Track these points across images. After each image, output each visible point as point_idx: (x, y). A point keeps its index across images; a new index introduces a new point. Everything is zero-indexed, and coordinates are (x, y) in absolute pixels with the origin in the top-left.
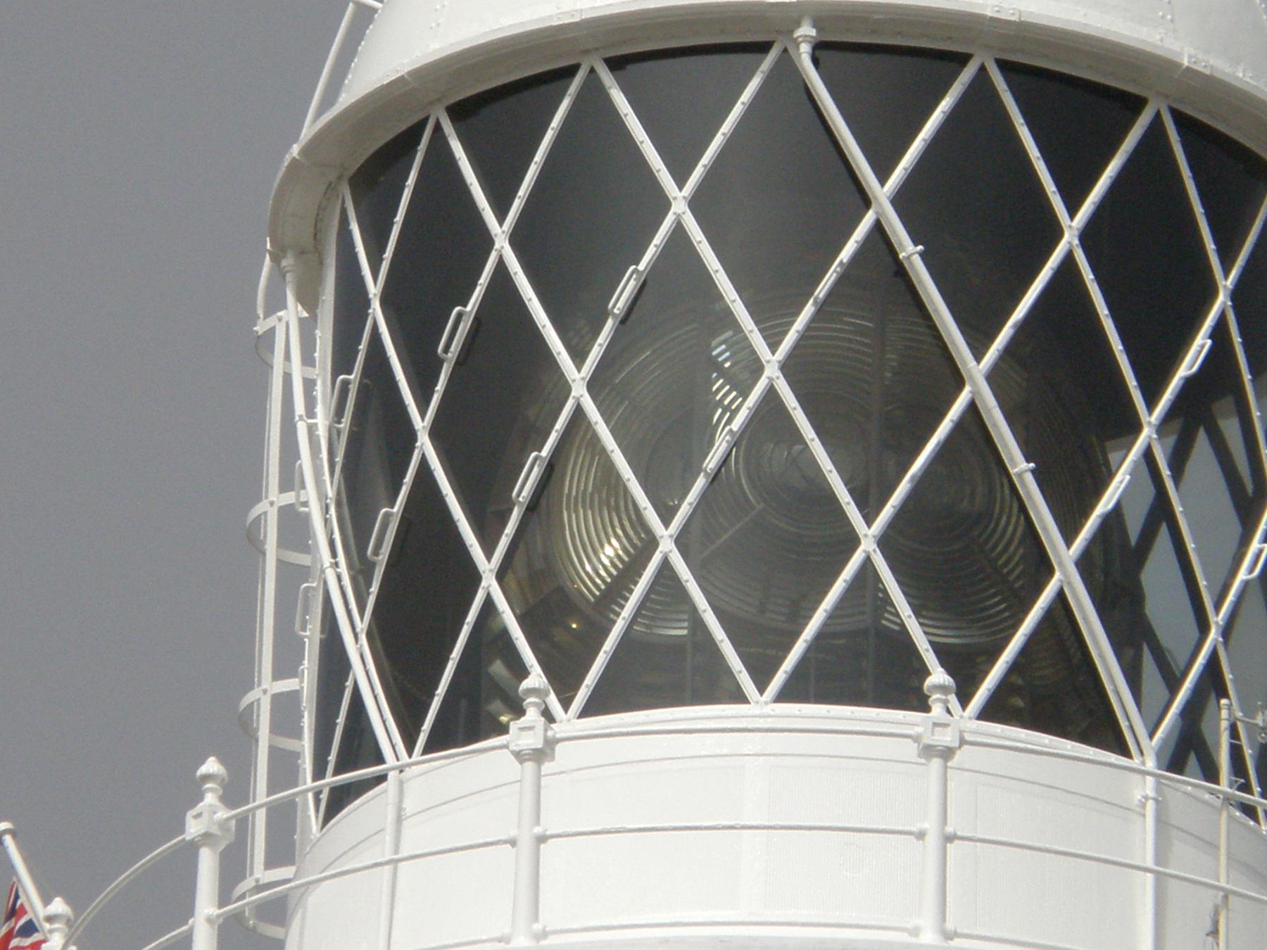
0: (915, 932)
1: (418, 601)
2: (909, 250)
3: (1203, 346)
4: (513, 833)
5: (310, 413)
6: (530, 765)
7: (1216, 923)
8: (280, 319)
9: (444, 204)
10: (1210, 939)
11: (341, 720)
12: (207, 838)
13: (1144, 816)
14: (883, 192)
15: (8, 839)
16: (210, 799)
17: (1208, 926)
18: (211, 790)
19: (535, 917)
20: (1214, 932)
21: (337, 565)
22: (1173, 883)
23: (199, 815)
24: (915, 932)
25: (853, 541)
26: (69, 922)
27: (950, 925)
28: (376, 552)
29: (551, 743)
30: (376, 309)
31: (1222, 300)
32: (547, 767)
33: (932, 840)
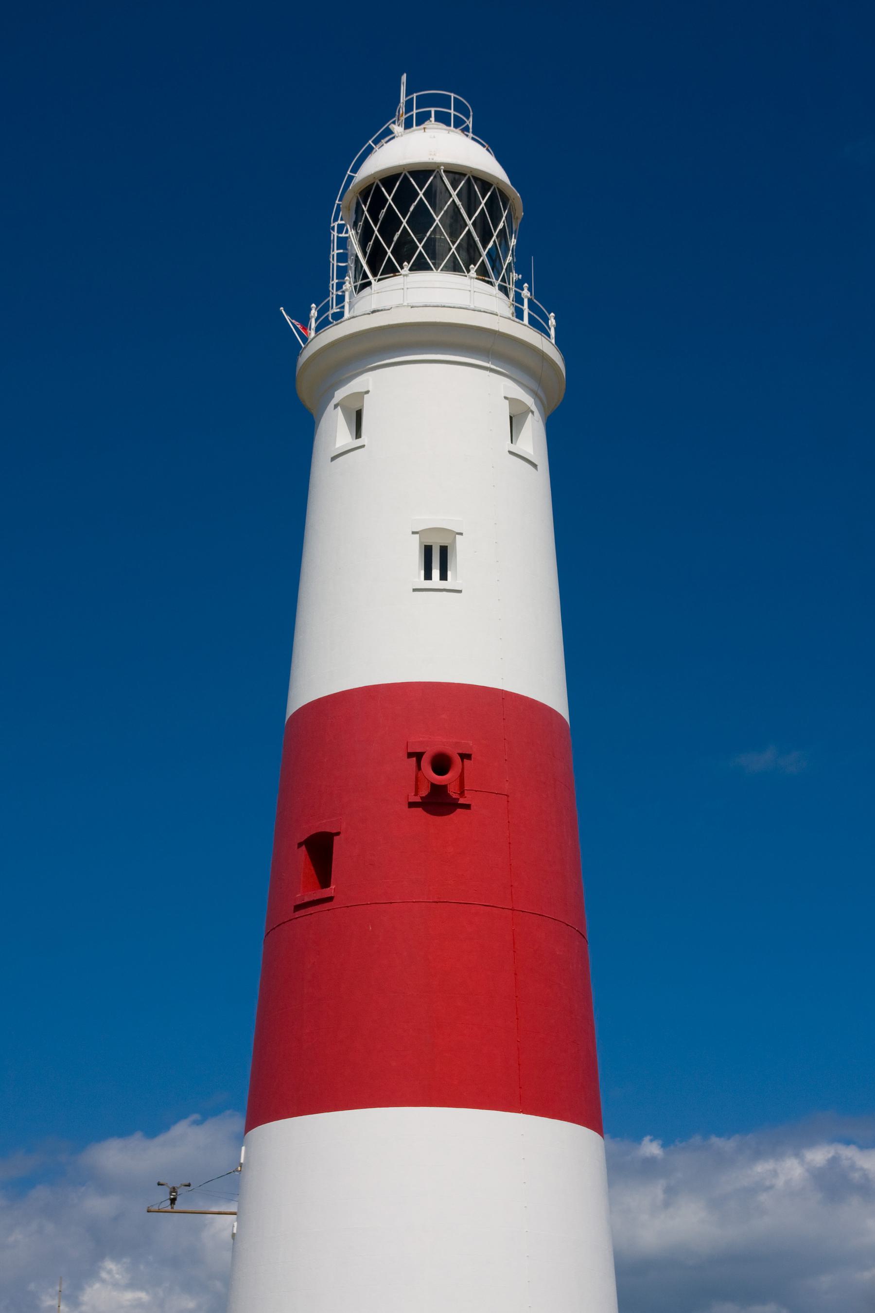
1: (375, 259)
31: (504, 218)
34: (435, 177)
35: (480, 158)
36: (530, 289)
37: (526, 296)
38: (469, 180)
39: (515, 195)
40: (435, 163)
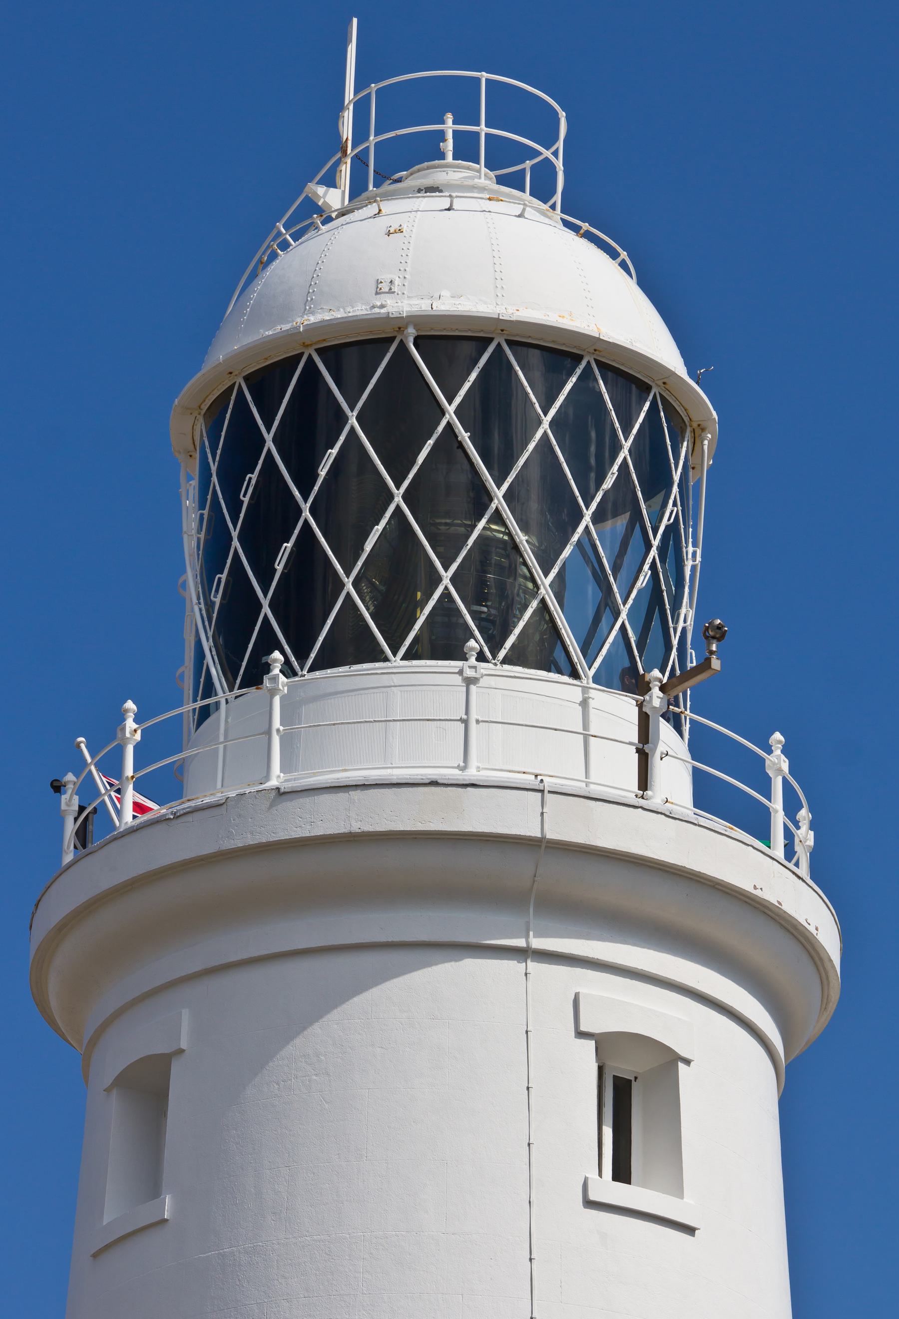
2: (464, 436)
11: (202, 680)
14: (451, 409)
21: (200, 603)
22: (592, 739)
28: (244, 496)
34: (654, 404)
35: (599, 299)
37: (779, 742)
38: (587, 374)
39: (703, 404)
40: (387, 319)
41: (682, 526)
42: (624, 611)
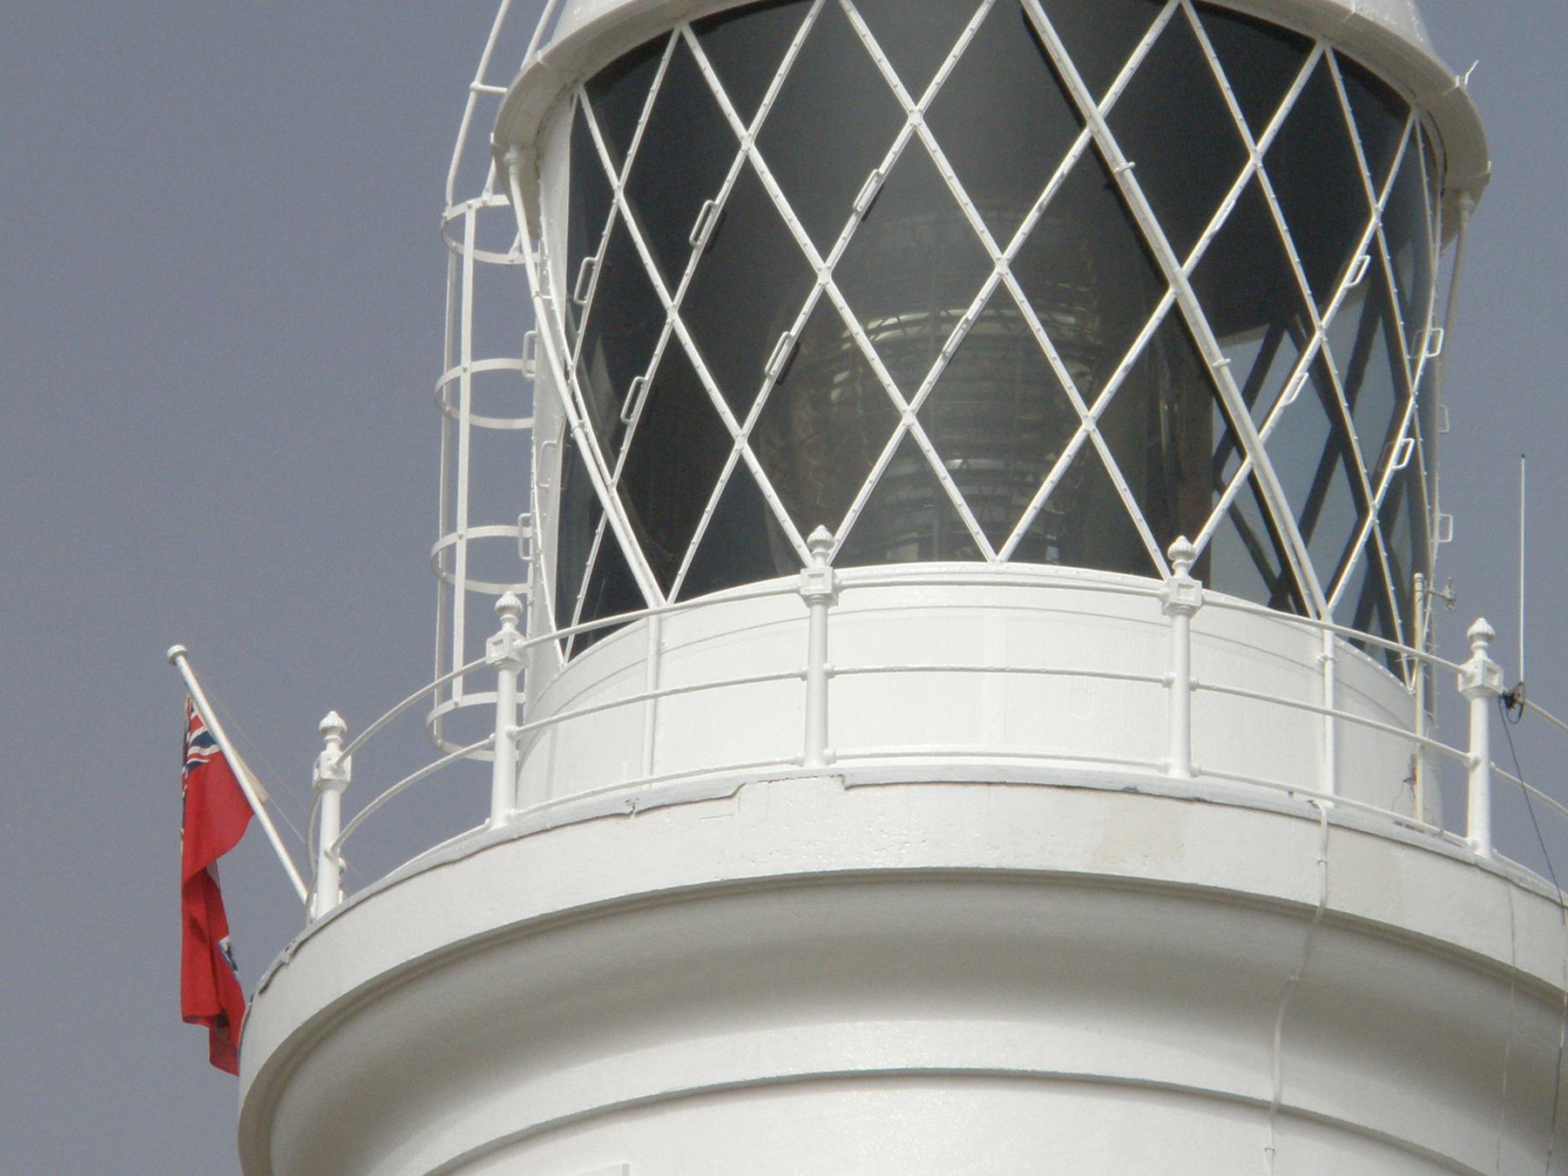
0: (1165, 769)
1: (669, 463)
2: (1121, 165)
3: (1362, 263)
4: (804, 669)
5: (544, 289)
6: (818, 609)
7: (1413, 770)
8: (470, 207)
9: (688, 112)
10: (1407, 785)
12: (507, 661)
13: (1323, 675)
14: (1097, 112)
15: (182, 661)
16: (508, 628)
17: (1406, 774)
18: (509, 620)
19: (825, 742)
20: (1412, 779)
23: (500, 642)
24: (1165, 769)
25: (1075, 422)
26: (342, 733)
27: (1195, 765)
28: (628, 415)
29: (837, 589)
30: (620, 200)
31: (1374, 221)
32: (832, 610)
33: (1179, 687)
36: (1499, 647)
41: (1424, 473)
42: (1322, 324)
